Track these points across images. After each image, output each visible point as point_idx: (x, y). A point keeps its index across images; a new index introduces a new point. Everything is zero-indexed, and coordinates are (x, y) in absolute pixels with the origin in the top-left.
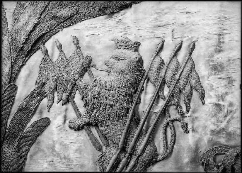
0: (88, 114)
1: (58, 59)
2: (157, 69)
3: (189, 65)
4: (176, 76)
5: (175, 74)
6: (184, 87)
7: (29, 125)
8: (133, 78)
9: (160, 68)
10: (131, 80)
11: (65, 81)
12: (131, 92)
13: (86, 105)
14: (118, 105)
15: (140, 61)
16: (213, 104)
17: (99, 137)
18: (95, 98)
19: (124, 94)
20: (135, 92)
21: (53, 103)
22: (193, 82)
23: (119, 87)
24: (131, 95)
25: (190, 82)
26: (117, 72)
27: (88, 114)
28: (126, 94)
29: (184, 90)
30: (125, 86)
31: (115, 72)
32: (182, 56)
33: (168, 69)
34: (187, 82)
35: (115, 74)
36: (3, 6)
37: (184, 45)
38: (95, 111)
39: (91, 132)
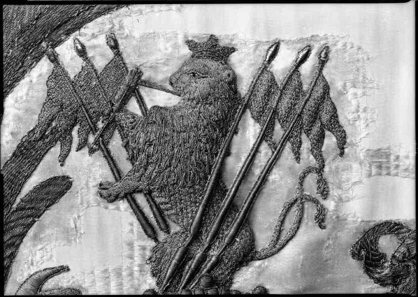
0: (137, 174)
1: (80, 72)
2: (265, 95)
3: (319, 91)
4: (297, 106)
5: (295, 105)
6: (311, 127)
7: (18, 200)
8: (221, 112)
9: (268, 94)
10: (218, 115)
11: (94, 112)
12: (217, 136)
13: (132, 159)
14: (193, 158)
15: (233, 81)
16: (140, 248)
17: (156, 224)
18: (152, 144)
19: (204, 140)
20: (224, 136)
21: (69, 150)
22: (325, 117)
23: (196, 126)
24: (215, 142)
25: (320, 119)
26: (193, 99)
27: (137, 174)
28: (207, 140)
29: (309, 132)
30: (208, 125)
31: (189, 99)
32: (307, 69)
33: (283, 95)
34: (316, 118)
35: (189, 103)
36: (48, 70)
37: (314, 52)
38: (150, 168)
39: (134, 201)
